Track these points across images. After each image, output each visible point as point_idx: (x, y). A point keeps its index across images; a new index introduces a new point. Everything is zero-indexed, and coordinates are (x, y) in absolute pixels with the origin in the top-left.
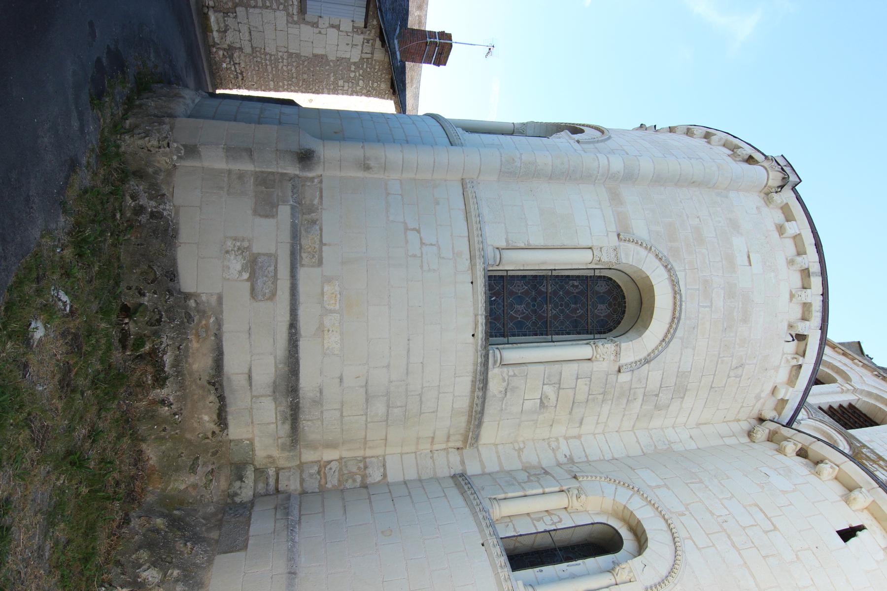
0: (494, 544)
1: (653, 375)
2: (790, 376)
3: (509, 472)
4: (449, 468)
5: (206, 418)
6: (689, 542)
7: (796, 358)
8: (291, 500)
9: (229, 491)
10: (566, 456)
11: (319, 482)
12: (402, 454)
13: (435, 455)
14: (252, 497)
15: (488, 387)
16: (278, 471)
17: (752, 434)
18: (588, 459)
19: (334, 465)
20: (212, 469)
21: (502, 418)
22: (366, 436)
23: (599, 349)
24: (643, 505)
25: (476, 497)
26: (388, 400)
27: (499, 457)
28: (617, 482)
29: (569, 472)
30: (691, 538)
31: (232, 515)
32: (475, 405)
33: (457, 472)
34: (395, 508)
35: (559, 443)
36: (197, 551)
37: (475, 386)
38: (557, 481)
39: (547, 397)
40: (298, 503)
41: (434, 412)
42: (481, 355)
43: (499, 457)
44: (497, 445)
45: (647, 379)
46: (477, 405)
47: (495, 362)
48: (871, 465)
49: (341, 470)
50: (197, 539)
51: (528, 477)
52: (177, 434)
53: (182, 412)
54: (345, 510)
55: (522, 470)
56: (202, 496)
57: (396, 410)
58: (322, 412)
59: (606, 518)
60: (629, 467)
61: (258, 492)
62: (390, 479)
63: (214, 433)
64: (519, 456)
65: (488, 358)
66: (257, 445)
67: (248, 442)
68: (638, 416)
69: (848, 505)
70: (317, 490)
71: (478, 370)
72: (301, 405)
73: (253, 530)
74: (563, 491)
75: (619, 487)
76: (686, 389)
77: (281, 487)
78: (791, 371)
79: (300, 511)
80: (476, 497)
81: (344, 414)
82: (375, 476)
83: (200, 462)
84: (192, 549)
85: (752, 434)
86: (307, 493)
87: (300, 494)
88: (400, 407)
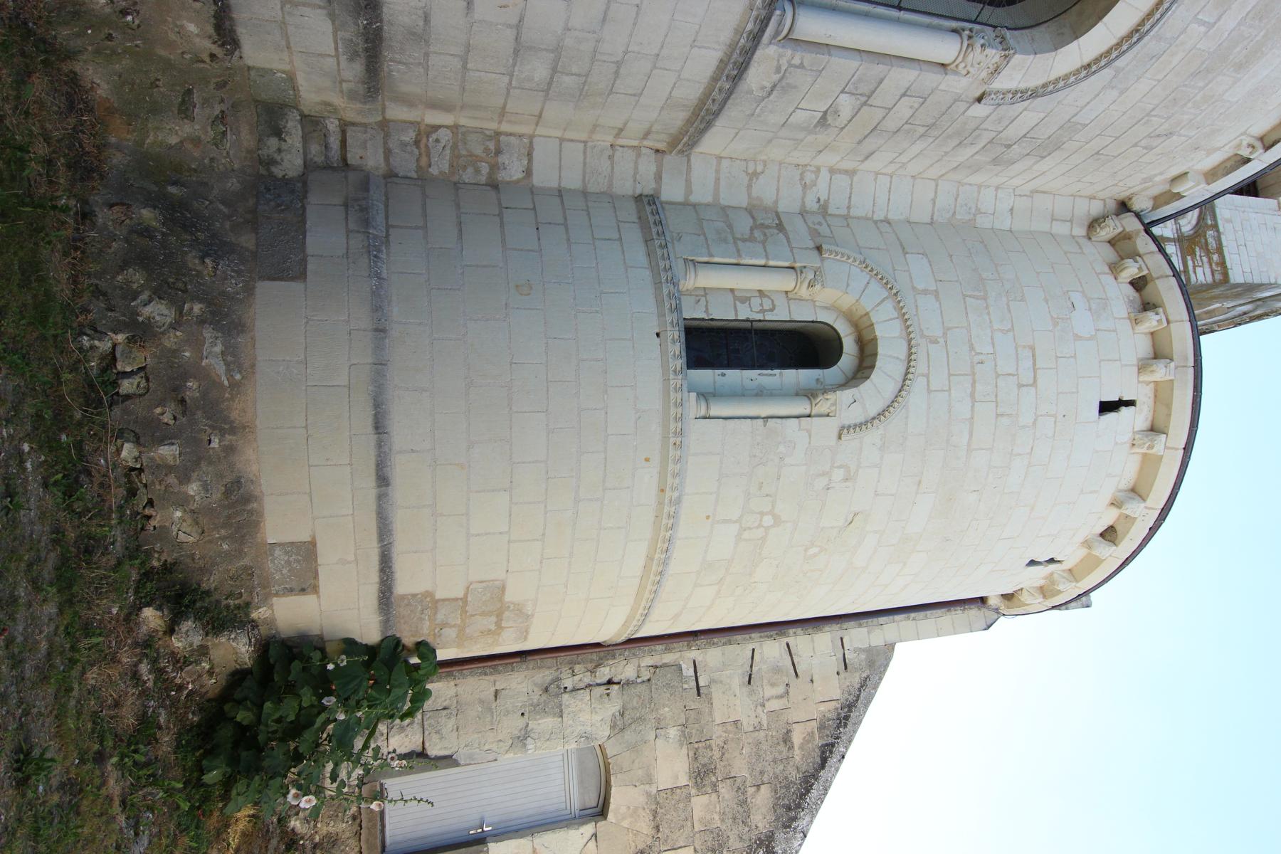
0: (674, 355)
1: (1028, 116)
2: (1219, 166)
3: (724, 210)
4: (635, 181)
5: (192, 28)
6: (922, 380)
7: (1253, 147)
8: (372, 192)
9: (260, 152)
10: (819, 199)
11: (418, 160)
12: (562, 140)
13: (618, 154)
14: (301, 169)
15: (744, 76)
16: (344, 126)
17: (1097, 225)
18: (849, 212)
19: (444, 135)
20: (222, 112)
21: (747, 127)
23: (972, 55)
24: (892, 317)
25: (666, 255)
26: (556, 60)
27: (717, 180)
28: (875, 272)
29: (814, 233)
30: (927, 376)
31: (272, 203)
32: (710, 101)
33: (647, 192)
34: (540, 245)
35: (817, 177)
36: (224, 272)
37: (723, 70)
38: (792, 249)
39: (836, 112)
40: (384, 198)
41: (634, 95)
42: (757, 18)
43: (717, 180)
44: (721, 158)
45: (1013, 121)
46: (714, 100)
47: (777, 33)
48: (1201, 257)
49: (455, 147)
50: (216, 248)
51: (752, 229)
52: (137, 46)
53: (137, 8)
54: (460, 230)
55: (746, 209)
56: (212, 160)
57: (567, 79)
58: (427, 55)
59: (834, 316)
60: (901, 245)
61: (311, 160)
62: (537, 180)
63: (213, 56)
64: (749, 187)
65: (767, 26)
66: (301, 80)
67: (284, 76)
68: (959, 165)
69: (1139, 373)
70: (414, 175)
71: (740, 44)
72: (385, 35)
73: (311, 246)
74: (793, 268)
75: (873, 279)
77: (352, 158)
78: (1229, 159)
79: (387, 218)
80: (666, 255)
81: (469, 66)
82: (513, 170)
83: (196, 97)
84: (215, 269)
85: (1097, 225)
86: (396, 176)
87: (385, 177)
88: (575, 75)
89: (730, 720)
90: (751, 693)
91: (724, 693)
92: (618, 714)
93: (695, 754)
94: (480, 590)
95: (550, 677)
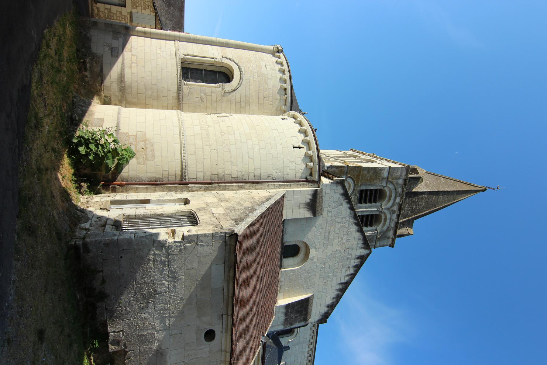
22: (145, 102)
39: (203, 97)
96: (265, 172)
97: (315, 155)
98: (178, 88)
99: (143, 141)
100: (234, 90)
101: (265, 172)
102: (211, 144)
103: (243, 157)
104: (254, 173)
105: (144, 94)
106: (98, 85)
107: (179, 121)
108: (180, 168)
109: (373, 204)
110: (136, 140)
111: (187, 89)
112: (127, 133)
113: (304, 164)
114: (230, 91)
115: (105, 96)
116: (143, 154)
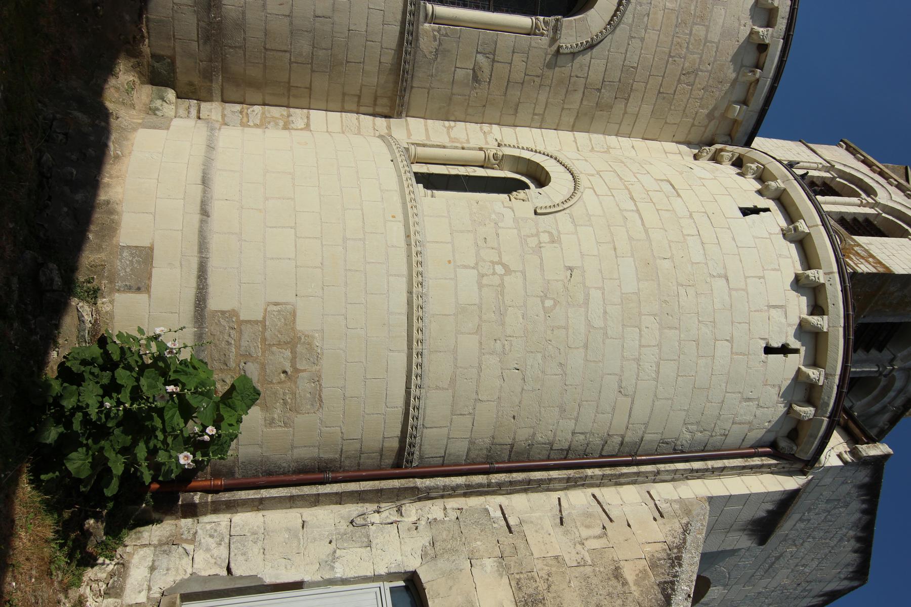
10: (496, 140)
22: (290, 79)
39: (480, 68)
48: (858, 260)
67: (169, 60)
68: (578, 113)
76: (631, 89)
89: (549, 555)
90: (566, 533)
91: (537, 531)
92: (428, 544)
93: (518, 584)
94: (275, 313)
95: (357, 512)
96: (657, 433)
97: (831, 388)
98: (402, 33)
99: (286, 343)
100: (591, 46)
101: (657, 433)
102: (507, 348)
103: (600, 392)
104: (623, 437)
105: (286, 51)
106: (127, 18)
107: (409, 245)
108: (398, 432)
109: (874, 352)
110: (264, 339)
111: (435, 37)
112: (234, 313)
113: (782, 405)
114: (576, 50)
115: (153, 56)
116: (284, 394)
